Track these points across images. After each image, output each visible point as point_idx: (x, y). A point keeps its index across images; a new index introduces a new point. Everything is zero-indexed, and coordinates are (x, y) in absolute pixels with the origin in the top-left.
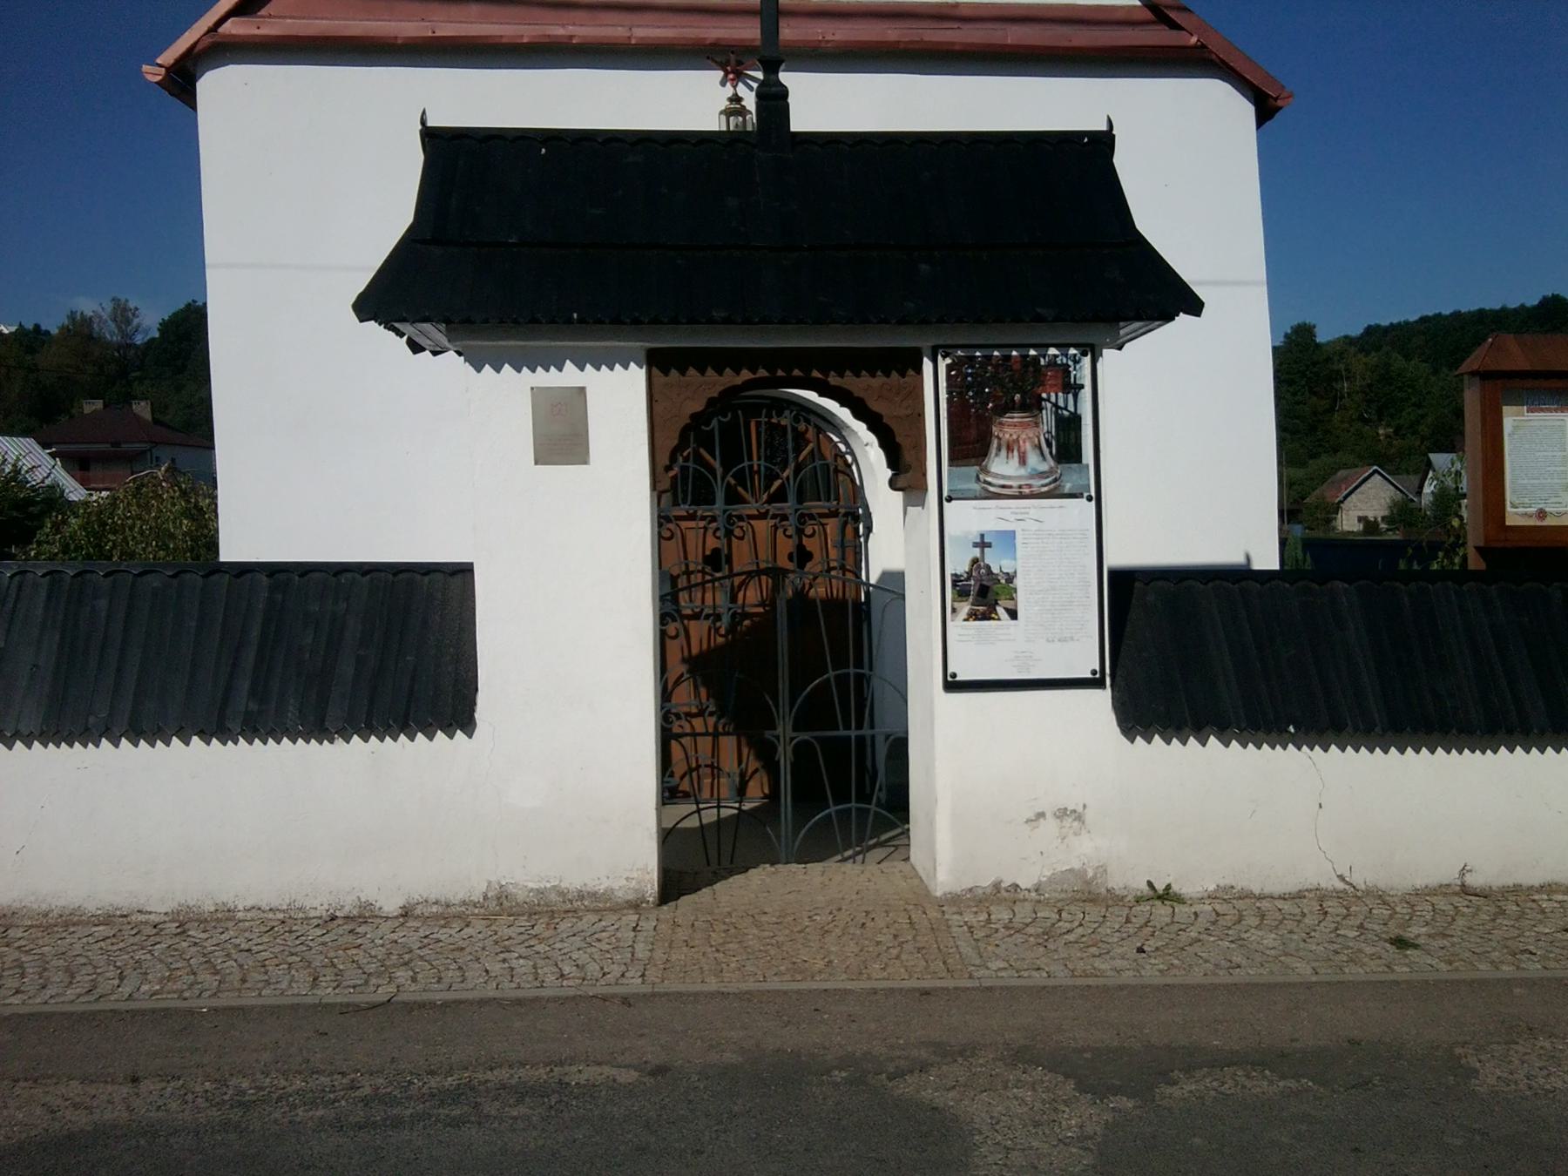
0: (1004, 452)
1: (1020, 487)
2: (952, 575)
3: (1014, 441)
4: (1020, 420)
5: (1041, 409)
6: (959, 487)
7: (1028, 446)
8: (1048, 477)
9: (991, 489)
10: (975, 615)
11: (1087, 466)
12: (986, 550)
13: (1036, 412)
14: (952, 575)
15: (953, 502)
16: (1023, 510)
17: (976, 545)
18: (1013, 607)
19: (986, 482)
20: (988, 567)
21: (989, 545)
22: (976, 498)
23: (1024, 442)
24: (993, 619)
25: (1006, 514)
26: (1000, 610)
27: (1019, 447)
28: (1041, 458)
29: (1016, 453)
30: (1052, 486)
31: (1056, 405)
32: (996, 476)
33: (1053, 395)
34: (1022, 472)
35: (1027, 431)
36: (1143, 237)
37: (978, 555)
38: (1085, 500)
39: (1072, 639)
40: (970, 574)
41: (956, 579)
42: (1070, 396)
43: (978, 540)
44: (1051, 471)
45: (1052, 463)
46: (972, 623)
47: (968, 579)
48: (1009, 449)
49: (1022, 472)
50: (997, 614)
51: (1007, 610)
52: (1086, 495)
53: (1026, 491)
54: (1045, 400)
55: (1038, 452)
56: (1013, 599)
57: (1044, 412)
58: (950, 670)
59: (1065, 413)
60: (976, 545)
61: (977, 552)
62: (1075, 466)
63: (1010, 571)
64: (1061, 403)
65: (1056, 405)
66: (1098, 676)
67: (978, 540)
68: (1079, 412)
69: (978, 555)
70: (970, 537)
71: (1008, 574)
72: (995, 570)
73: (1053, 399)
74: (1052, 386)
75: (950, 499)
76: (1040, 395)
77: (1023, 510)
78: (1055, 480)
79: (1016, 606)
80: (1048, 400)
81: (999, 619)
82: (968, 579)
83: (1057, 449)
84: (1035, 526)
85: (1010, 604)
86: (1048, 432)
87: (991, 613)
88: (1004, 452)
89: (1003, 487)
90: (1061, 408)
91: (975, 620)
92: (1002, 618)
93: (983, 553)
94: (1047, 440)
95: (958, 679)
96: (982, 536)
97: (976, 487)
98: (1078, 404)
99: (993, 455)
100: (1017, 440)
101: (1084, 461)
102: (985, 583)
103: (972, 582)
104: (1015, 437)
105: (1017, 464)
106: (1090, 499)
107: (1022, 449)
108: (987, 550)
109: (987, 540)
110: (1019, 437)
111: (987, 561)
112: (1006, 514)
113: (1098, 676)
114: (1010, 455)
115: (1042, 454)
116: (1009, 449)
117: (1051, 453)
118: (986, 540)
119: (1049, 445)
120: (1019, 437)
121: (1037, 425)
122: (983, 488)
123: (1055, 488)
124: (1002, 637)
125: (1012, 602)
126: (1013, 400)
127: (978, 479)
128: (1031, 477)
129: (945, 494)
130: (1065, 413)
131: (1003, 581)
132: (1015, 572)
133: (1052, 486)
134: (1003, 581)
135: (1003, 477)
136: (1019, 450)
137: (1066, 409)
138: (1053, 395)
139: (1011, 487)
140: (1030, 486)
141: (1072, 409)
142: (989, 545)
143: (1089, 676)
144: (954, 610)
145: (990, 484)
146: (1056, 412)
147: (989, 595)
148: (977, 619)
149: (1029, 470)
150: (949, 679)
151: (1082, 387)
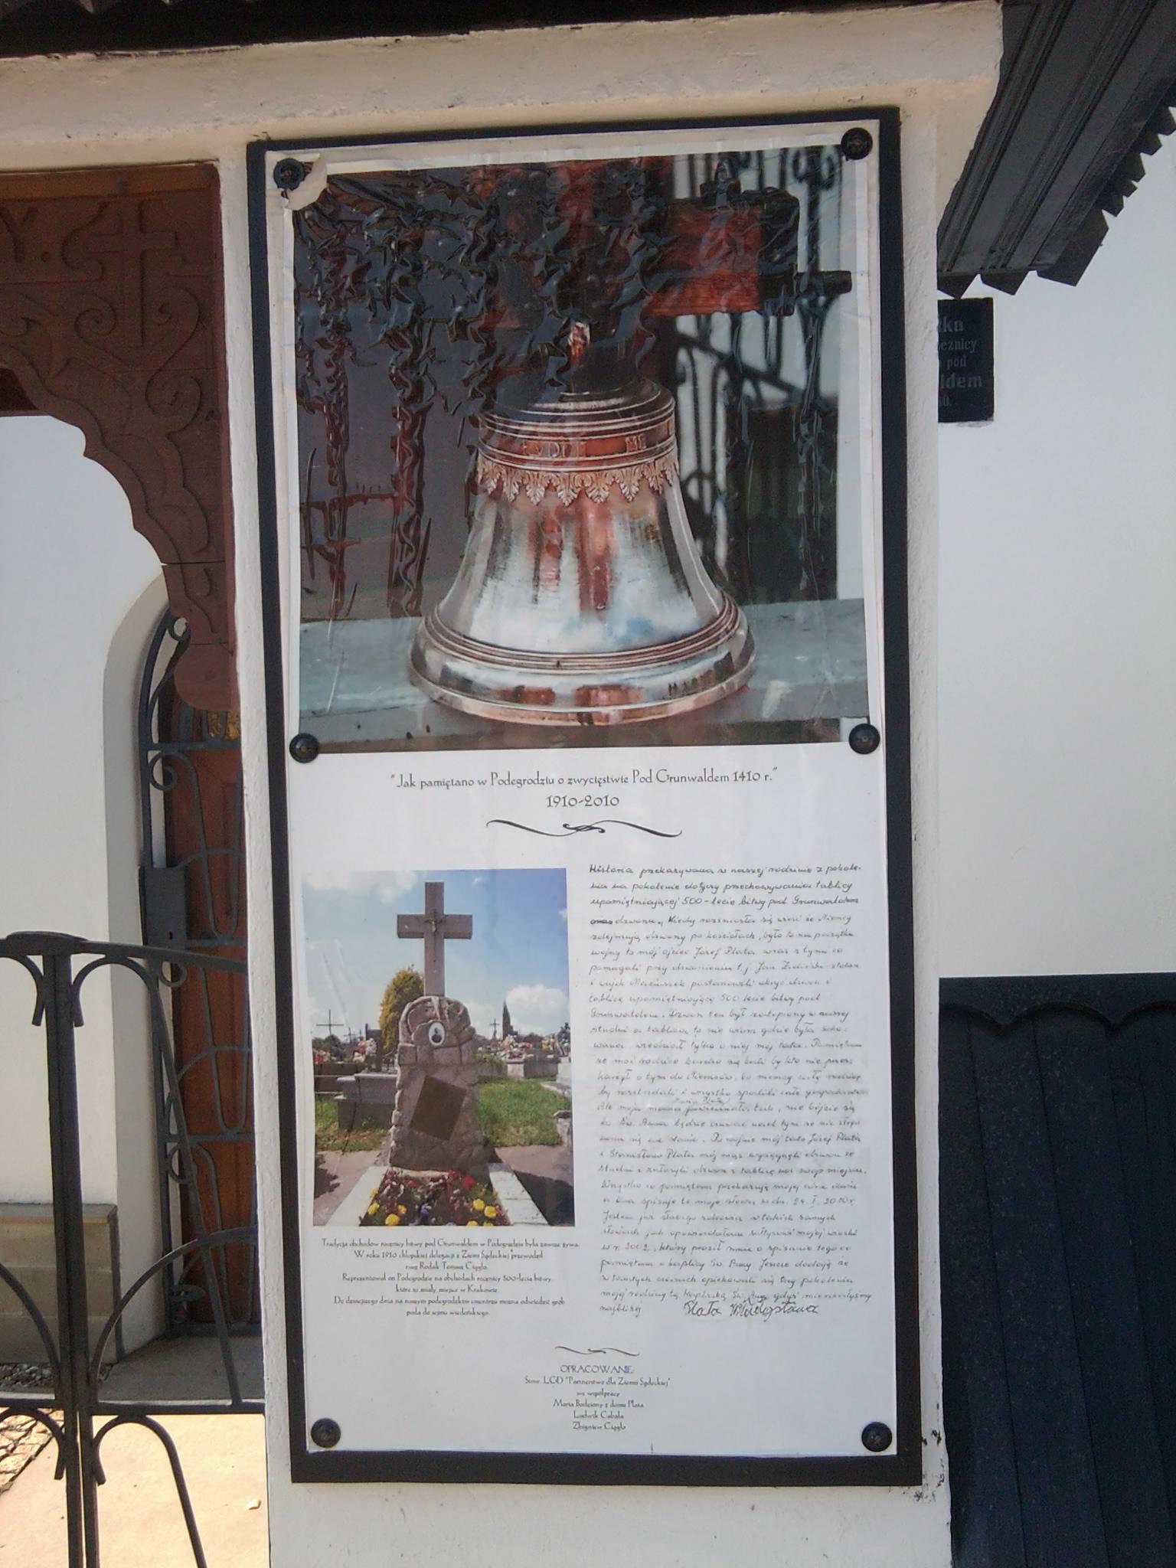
0: (520, 561)
1: (585, 696)
2: (317, 1044)
3: (561, 513)
4: (586, 427)
5: (671, 380)
6: (346, 699)
7: (618, 537)
8: (692, 659)
9: (471, 706)
10: (406, 1200)
11: (857, 608)
12: (450, 946)
13: (652, 391)
14: (317, 1044)
15: (322, 758)
16: (595, 791)
17: (407, 927)
18: (554, 1175)
19: (448, 679)
20: (457, 1016)
21: (461, 928)
22: (408, 743)
23: (604, 516)
24: (481, 1219)
25: (530, 805)
26: (505, 1185)
27: (582, 539)
28: (669, 580)
29: (568, 562)
30: (711, 693)
31: (731, 364)
32: (490, 653)
33: (721, 322)
34: (593, 635)
35: (615, 471)
36: (292, 1034)
37: (419, 968)
38: (844, 746)
39: (788, 1305)
40: (384, 1039)
41: (329, 1049)
42: (793, 325)
43: (418, 908)
44: (706, 635)
45: (712, 597)
46: (391, 1233)
47: (380, 1059)
48: (544, 546)
49: (593, 635)
50: (490, 1197)
51: (534, 1186)
52: (847, 725)
53: (610, 712)
54: (687, 342)
55: (658, 555)
56: (555, 1142)
57: (685, 393)
58: (313, 1415)
59: (770, 392)
60: (407, 927)
61: (412, 955)
62: (801, 610)
63: (545, 1029)
64: (753, 355)
65: (731, 364)
66: (892, 1450)
67: (418, 908)
68: (826, 388)
69: (419, 968)
70: (388, 894)
71: (533, 1039)
72: (484, 1024)
73: (720, 340)
74: (718, 285)
75: (308, 748)
76: (671, 322)
77: (595, 791)
78: (725, 669)
79: (568, 1168)
80: (702, 342)
81: (500, 1220)
82: (380, 1059)
83: (733, 548)
84: (640, 850)
85: (542, 1163)
86: (698, 474)
87: (468, 1194)
88: (520, 561)
89: (518, 695)
90: (754, 376)
91: (403, 1222)
92: (511, 1217)
93: (434, 958)
94: (693, 509)
95: (341, 1446)
96: (434, 891)
97: (413, 699)
98: (688, 633)
99: (480, 567)
100: (574, 513)
101: (845, 588)
102: (444, 1076)
103: (397, 1073)
104: (565, 495)
105: (574, 605)
106: (863, 741)
107: (595, 544)
108: (451, 947)
109: (451, 907)
110: (582, 494)
111: (450, 994)
112: (530, 805)
113: (892, 1450)
114: (547, 571)
115: (674, 563)
116: (544, 546)
117: (708, 559)
118: (450, 908)
119: (702, 526)
120: (582, 494)
121: (652, 443)
122: (439, 702)
123: (720, 704)
124: (505, 1291)
125: (553, 1155)
126: (558, 345)
127: (418, 663)
128: (630, 654)
129: (292, 728)
130: (770, 392)
131: (516, 1070)
132: (565, 1034)
133: (711, 693)
134: (516, 1070)
135: (520, 658)
136: (580, 554)
137: (772, 375)
138: (721, 322)
139: (546, 697)
140: (620, 692)
141: (794, 371)
142: (461, 928)
143: (857, 1449)
144: (324, 1183)
145: (465, 686)
146: (735, 386)
147: (460, 1127)
148: (417, 1216)
149: (621, 630)
150: (312, 1447)
151: (841, 283)
